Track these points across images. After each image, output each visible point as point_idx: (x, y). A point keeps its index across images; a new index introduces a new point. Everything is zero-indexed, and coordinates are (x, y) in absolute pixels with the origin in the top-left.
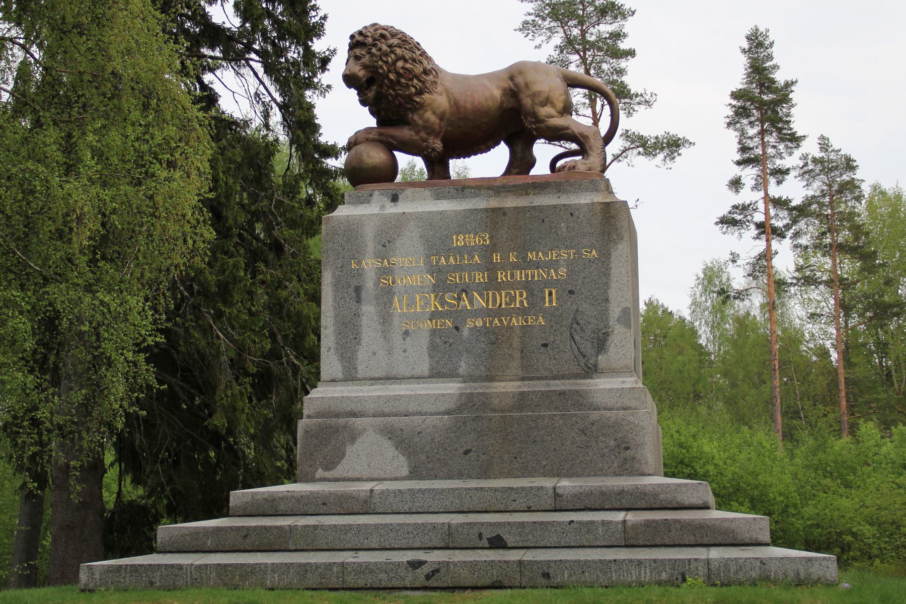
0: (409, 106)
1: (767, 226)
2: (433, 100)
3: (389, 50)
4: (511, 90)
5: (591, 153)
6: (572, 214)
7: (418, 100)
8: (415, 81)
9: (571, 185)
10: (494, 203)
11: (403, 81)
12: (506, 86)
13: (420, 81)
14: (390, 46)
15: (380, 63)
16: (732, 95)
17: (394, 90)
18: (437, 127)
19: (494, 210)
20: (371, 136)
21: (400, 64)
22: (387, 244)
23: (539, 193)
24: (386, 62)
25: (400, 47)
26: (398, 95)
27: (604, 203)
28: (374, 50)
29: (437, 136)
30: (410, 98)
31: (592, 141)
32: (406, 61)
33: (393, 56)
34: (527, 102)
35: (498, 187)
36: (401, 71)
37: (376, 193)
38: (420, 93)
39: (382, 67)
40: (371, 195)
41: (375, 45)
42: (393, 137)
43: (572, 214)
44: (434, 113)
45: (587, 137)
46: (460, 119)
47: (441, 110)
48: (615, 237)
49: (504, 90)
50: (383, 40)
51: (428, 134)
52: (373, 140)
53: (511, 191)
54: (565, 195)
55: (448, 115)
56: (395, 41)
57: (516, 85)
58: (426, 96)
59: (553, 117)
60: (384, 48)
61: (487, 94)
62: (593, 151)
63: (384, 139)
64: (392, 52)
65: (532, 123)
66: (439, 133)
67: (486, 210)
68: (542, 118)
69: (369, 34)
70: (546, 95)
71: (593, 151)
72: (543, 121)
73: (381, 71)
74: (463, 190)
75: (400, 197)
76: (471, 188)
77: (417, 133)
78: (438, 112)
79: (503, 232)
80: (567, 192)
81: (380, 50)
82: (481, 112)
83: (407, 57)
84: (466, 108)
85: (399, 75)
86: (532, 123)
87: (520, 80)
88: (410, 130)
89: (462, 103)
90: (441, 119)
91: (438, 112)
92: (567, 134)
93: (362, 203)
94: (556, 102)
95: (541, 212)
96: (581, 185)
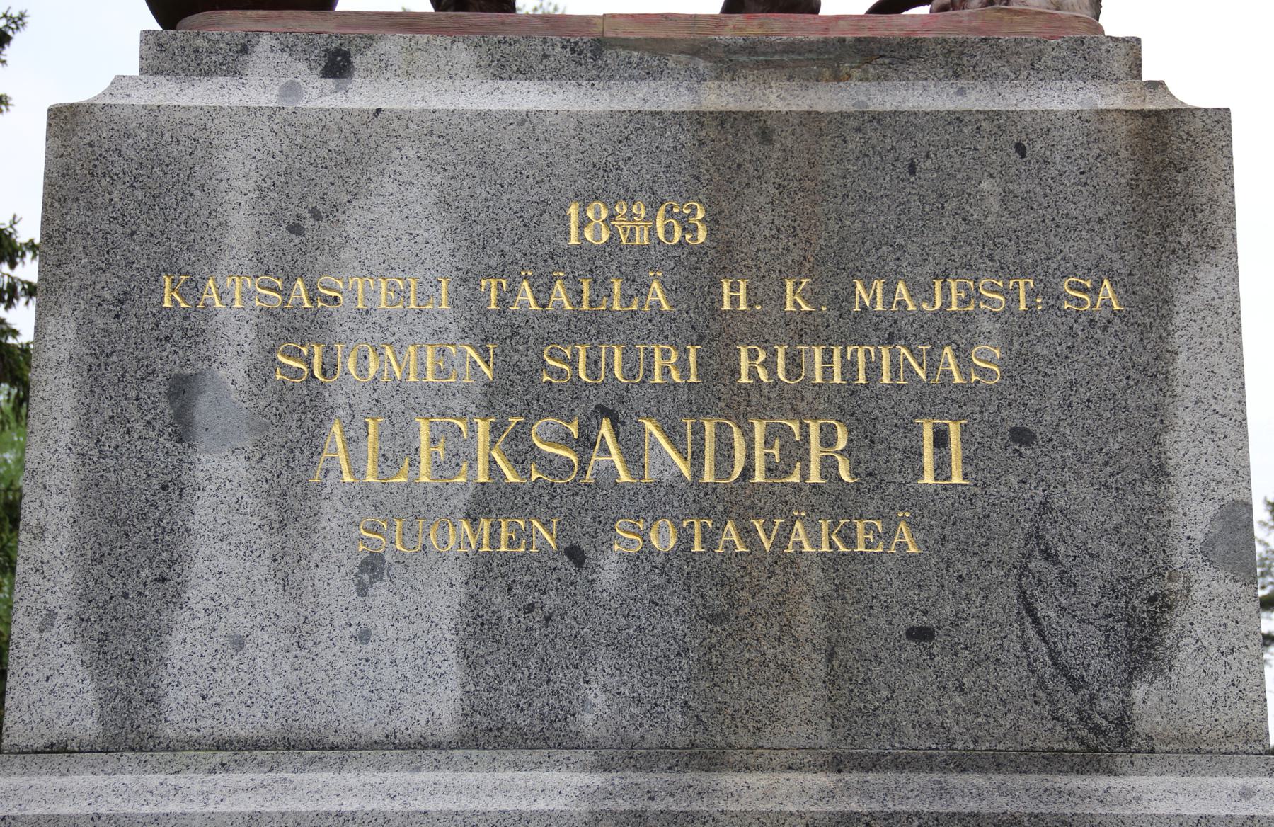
35: (728, 49)
40: (244, 50)
67: (698, 118)
75: (357, 60)
80: (988, 76)
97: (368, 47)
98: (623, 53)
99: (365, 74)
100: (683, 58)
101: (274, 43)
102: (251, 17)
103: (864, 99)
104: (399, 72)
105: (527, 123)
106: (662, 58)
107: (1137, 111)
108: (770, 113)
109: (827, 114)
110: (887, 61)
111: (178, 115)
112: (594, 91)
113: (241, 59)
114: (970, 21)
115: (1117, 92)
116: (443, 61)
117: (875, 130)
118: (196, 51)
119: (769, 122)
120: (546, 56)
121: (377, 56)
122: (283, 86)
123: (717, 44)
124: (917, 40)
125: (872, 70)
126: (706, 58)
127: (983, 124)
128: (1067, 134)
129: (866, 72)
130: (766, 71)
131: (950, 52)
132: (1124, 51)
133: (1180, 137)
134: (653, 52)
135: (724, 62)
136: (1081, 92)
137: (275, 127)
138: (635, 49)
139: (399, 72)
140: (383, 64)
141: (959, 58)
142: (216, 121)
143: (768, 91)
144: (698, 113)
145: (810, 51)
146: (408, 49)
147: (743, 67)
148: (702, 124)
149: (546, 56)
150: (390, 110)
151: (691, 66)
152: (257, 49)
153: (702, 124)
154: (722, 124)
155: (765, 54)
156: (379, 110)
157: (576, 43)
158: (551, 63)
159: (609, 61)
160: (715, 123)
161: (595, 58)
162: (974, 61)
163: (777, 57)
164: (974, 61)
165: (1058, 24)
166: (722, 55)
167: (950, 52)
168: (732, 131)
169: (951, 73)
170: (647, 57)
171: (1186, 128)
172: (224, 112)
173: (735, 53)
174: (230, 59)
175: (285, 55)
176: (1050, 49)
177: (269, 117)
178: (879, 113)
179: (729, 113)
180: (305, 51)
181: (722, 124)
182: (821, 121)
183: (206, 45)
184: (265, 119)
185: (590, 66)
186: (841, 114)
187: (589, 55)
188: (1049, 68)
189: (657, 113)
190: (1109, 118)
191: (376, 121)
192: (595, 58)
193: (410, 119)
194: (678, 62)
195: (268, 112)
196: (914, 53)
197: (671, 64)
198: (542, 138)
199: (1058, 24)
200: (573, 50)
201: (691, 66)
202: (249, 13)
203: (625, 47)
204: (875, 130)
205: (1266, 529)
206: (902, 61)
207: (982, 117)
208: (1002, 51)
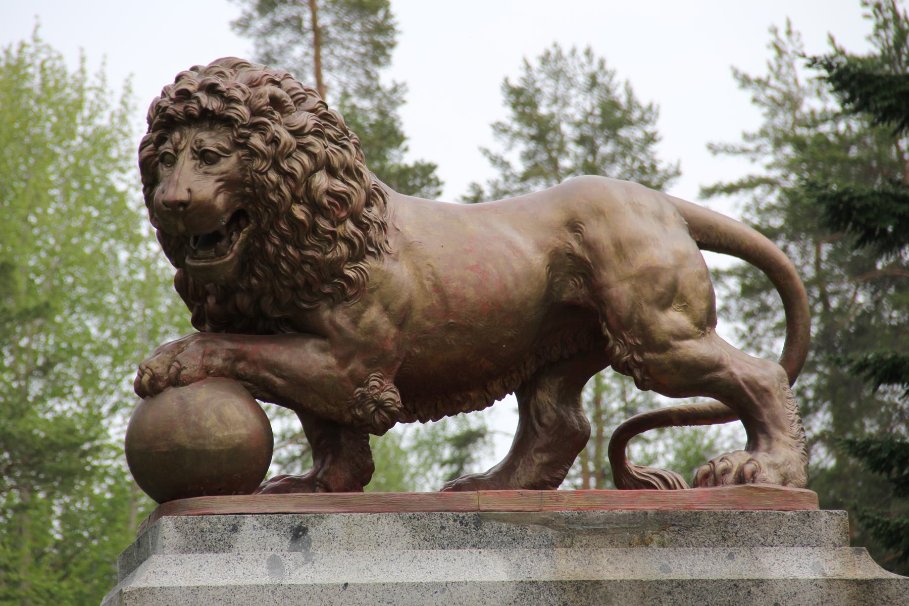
0: (327, 289)
1: (422, 460)
2: (387, 276)
3: (294, 142)
4: (572, 255)
5: (777, 433)
7: (351, 274)
8: (350, 225)
9: (754, 523)
10: (568, 565)
11: (324, 224)
12: (558, 243)
14: (297, 133)
15: (273, 176)
16: (657, 137)
17: (299, 246)
18: (391, 346)
19: (579, 586)
23: (674, 543)
24: (288, 175)
26: (305, 260)
27: (858, 582)
28: (256, 141)
30: (334, 270)
31: (778, 402)
32: (332, 172)
33: (305, 158)
34: (621, 291)
35: (568, 520)
36: (325, 200)
38: (358, 253)
39: (277, 187)
40: (235, 529)
41: (258, 127)
42: (273, 367)
44: (386, 309)
45: (766, 390)
46: (450, 328)
50: (277, 115)
53: (603, 532)
54: (744, 551)
55: (417, 317)
57: (588, 245)
58: (370, 264)
59: (686, 336)
60: (286, 137)
61: (518, 267)
62: (782, 429)
63: (250, 371)
64: (302, 148)
65: (632, 349)
67: (561, 586)
68: (660, 337)
69: (238, 94)
70: (666, 279)
71: (782, 429)
72: (664, 347)
73: (274, 198)
74: (478, 524)
75: (312, 532)
76: (499, 519)
78: (396, 306)
80: (749, 543)
81: (275, 141)
82: (499, 311)
83: (336, 162)
84: (465, 300)
85: (316, 208)
86: (632, 349)
87: (597, 231)
88: (324, 350)
89: (452, 287)
92: (719, 380)
93: (210, 549)
94: (691, 296)
96: (780, 524)
97: (319, 523)
98: (496, 524)
99: (319, 544)
100: (537, 527)
101: (256, 523)
102: (234, 501)
103: (666, 562)
104: (342, 542)
105: (447, 592)
106: (523, 529)
107: (854, 580)
108: (610, 581)
109: (648, 582)
110: (677, 529)
111: (211, 592)
112: (482, 558)
113: (233, 536)
114: (730, 496)
115: (835, 558)
116: (372, 533)
117: (680, 593)
118: (202, 531)
119: (609, 588)
120: (443, 528)
121: (326, 531)
122: (269, 560)
123: (559, 517)
124: (696, 513)
125: (666, 535)
126: (553, 528)
127: (752, 589)
128: (808, 596)
129: (663, 536)
130: (595, 537)
131: (719, 522)
132: (836, 522)
133: (882, 599)
134: (516, 523)
135: (565, 530)
136: (811, 557)
137: (277, 599)
138: (504, 521)
139: (342, 542)
140: (331, 536)
141: (726, 527)
142: (237, 596)
143: (600, 556)
144: (561, 582)
145: (625, 522)
146: (347, 525)
147: (579, 534)
148: (564, 590)
149: (443, 528)
150: (354, 585)
151: (543, 533)
152: (244, 528)
153: (564, 590)
154: (577, 590)
155: (594, 525)
156: (346, 585)
157: (463, 517)
158: (447, 533)
159: (487, 530)
160: (573, 589)
161: (477, 528)
162: (736, 528)
163: (601, 527)
164: (736, 528)
165: (790, 498)
166: (564, 525)
167: (719, 522)
168: (585, 594)
169: (720, 538)
170: (513, 527)
171: (886, 593)
172: (242, 590)
173: (573, 523)
174: (225, 536)
175: (264, 532)
176: (787, 520)
177: (273, 592)
178: (683, 581)
179: (582, 582)
180: (276, 528)
181: (577, 590)
182: (644, 587)
183: (209, 526)
184: (270, 593)
185: (474, 535)
186: (657, 581)
187: (473, 526)
188: (786, 534)
189: (534, 582)
190: (835, 585)
191: (345, 593)
192: (477, 528)
193: (368, 590)
194: (534, 531)
195: (271, 588)
196: (695, 523)
197: (529, 532)
198: (457, 602)
199: (790, 498)
200: (461, 522)
201: (543, 533)
202: (233, 497)
203: (497, 520)
204: (680, 593)
205: (506, 138)
206: (687, 528)
207: (750, 583)
208: (755, 522)
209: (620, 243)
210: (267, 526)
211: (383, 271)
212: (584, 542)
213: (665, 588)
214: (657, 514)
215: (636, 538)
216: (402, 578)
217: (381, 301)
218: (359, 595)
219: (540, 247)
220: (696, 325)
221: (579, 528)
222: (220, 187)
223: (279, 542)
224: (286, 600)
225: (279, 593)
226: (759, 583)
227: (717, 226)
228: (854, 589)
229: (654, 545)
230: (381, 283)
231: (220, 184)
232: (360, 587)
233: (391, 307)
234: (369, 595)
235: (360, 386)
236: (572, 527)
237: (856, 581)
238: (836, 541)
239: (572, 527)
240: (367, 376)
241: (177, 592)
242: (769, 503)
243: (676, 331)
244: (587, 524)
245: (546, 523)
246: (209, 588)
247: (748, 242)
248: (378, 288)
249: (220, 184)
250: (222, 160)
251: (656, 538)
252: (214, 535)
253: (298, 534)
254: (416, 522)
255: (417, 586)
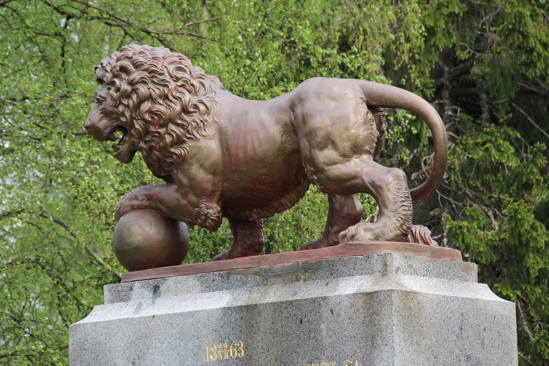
3: (129, 88)
6: (332, 311)
7: (177, 151)
13: (178, 125)
20: (136, 202)
21: (146, 106)
22: (137, 361)
25: (144, 82)
27: (367, 294)
29: (210, 196)
34: (304, 144)
37: (137, 284)
38: (179, 142)
39: (123, 114)
40: (131, 289)
43: (332, 311)
44: (202, 166)
45: (380, 187)
47: (210, 161)
48: (379, 342)
49: (285, 125)
50: (124, 76)
51: (197, 196)
52: (140, 208)
56: (136, 75)
59: (334, 163)
60: (125, 87)
63: (154, 205)
66: (213, 192)
74: (228, 277)
75: (161, 288)
76: (237, 274)
77: (184, 195)
78: (207, 164)
79: (259, 338)
81: (118, 90)
82: (259, 161)
90: (214, 173)
91: (207, 164)
94: (338, 141)
95: (299, 309)
100: (253, 276)
109: (277, 303)
116: (185, 286)
120: (214, 280)
129: (305, 275)
133: (377, 302)
134: (244, 274)
135: (264, 276)
138: (239, 274)
150: (157, 316)
155: (276, 272)
156: (154, 316)
158: (215, 283)
163: (279, 273)
191: (153, 320)
195: (125, 320)
197: (249, 279)
207: (320, 299)
209: (262, 122)
210: (144, 286)
211: (198, 147)
212: (272, 282)
213: (284, 306)
214: (303, 263)
215: (294, 277)
216: (177, 310)
217: (198, 162)
218: (159, 321)
219: (277, 122)
220: (341, 156)
221: (270, 274)
222: (102, 117)
223: (148, 293)
224: (130, 326)
225: (127, 323)
226: (324, 298)
227: (384, 95)
228: (365, 298)
229: (302, 281)
230: (197, 153)
231: (102, 115)
232: (159, 317)
233: (204, 165)
234: (163, 321)
235: (196, 207)
236: (267, 274)
237: (366, 293)
238: (381, 270)
239: (267, 274)
240: (198, 202)
241: (89, 325)
242: (356, 252)
243: (327, 161)
244: (274, 272)
245: (256, 274)
246: (101, 322)
247: (402, 102)
248: (195, 156)
249: (102, 115)
250: (103, 102)
251: (303, 277)
252: (123, 293)
253: (156, 289)
254: (203, 279)
255: (182, 314)
